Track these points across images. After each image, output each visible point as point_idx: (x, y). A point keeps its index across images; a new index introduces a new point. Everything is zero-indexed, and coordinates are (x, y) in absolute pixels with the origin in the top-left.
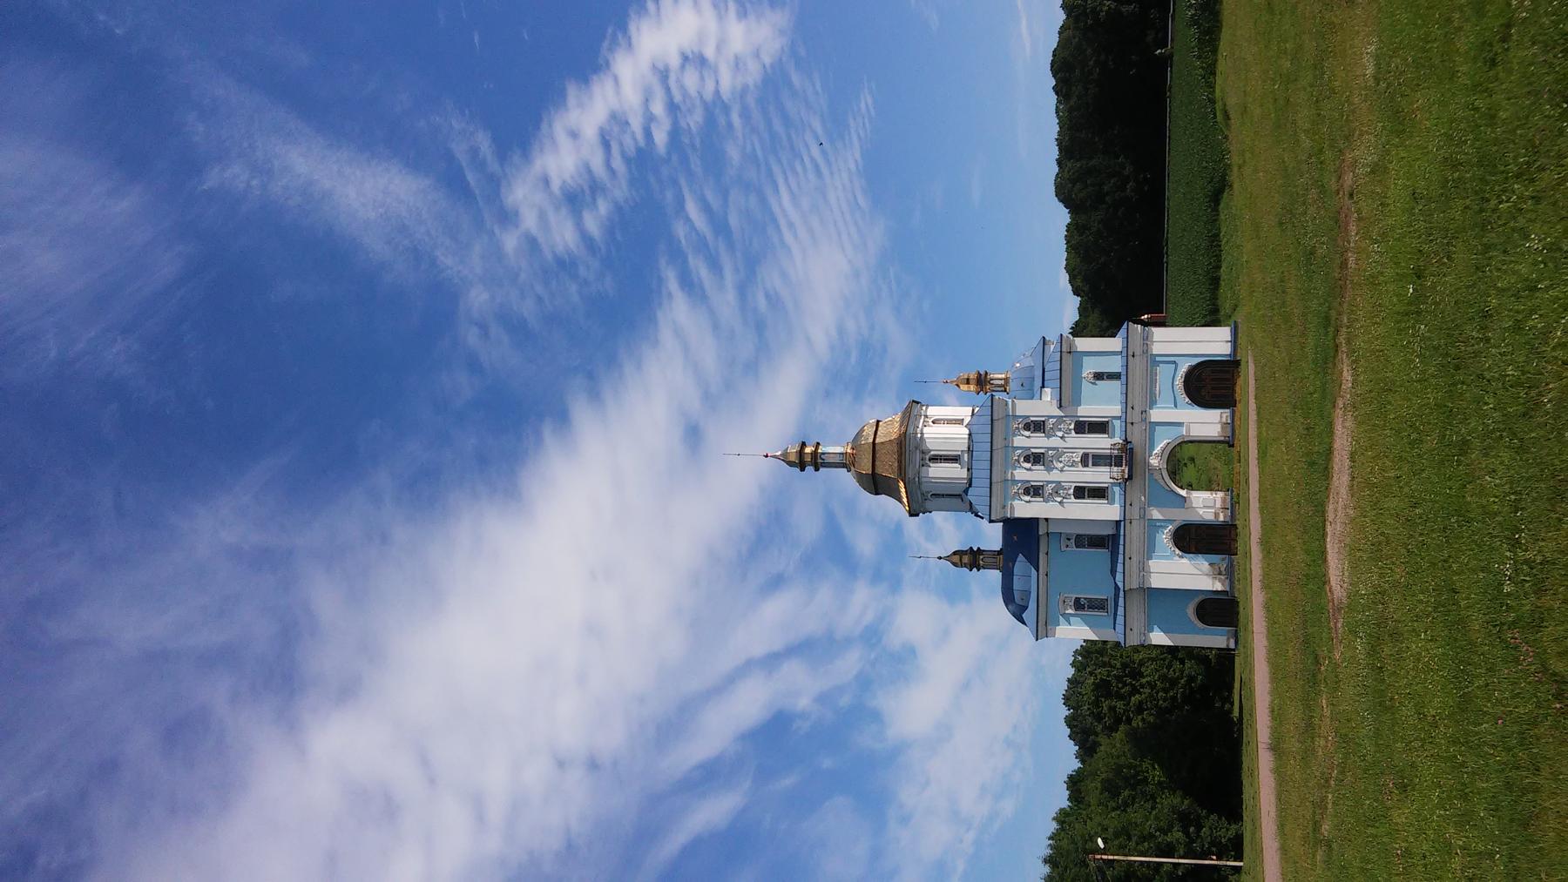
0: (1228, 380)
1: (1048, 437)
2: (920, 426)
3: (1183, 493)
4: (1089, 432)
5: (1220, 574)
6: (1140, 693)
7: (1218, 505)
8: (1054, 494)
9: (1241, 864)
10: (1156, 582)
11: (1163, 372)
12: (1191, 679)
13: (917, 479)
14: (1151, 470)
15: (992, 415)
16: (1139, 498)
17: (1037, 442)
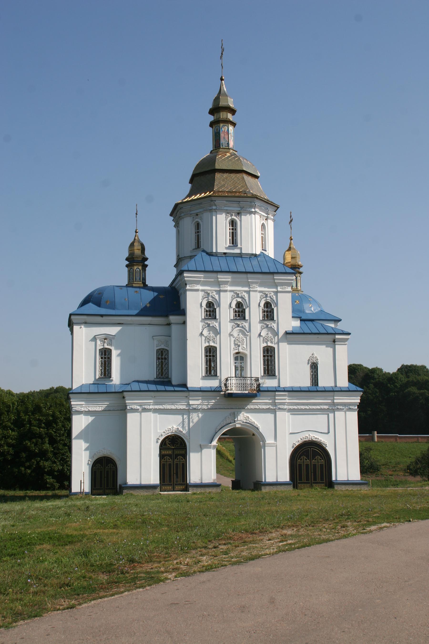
0: (315, 479)
14: (235, 415)
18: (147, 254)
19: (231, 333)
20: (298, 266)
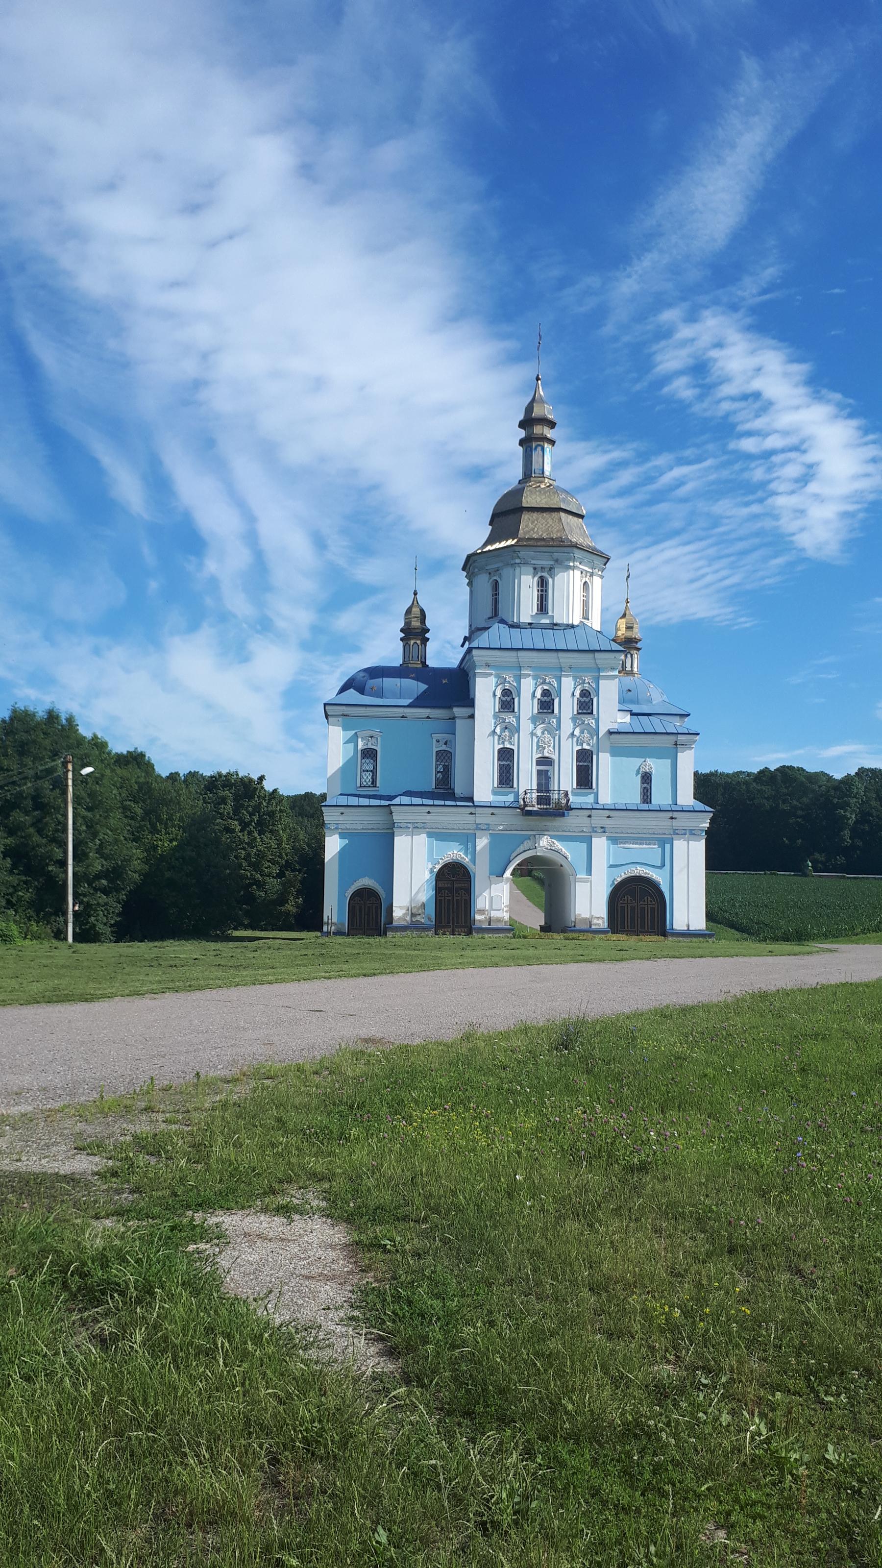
1: (574, 719)
2: (581, 567)
3: (508, 874)
4: (578, 767)
5: (413, 915)
6: (242, 831)
7: (494, 914)
8: (504, 725)
9: (70, 939)
10: (401, 843)
11: (652, 852)
12: (260, 885)
13: (518, 561)
14: (534, 838)
15: (600, 651)
16: (502, 822)
17: (567, 706)
18: (429, 623)
19: (534, 732)
20: (635, 638)
